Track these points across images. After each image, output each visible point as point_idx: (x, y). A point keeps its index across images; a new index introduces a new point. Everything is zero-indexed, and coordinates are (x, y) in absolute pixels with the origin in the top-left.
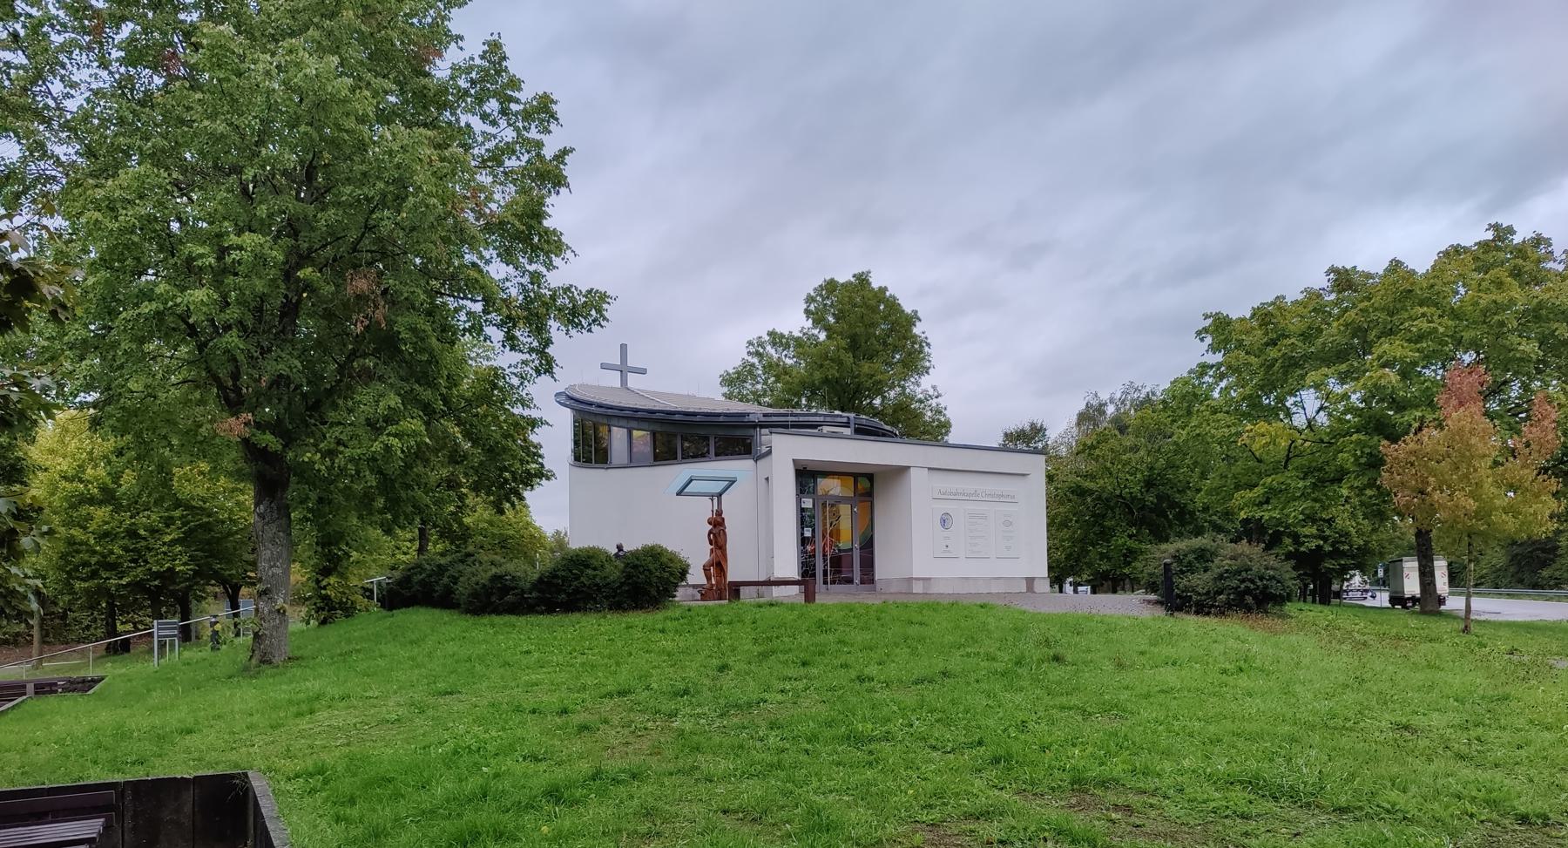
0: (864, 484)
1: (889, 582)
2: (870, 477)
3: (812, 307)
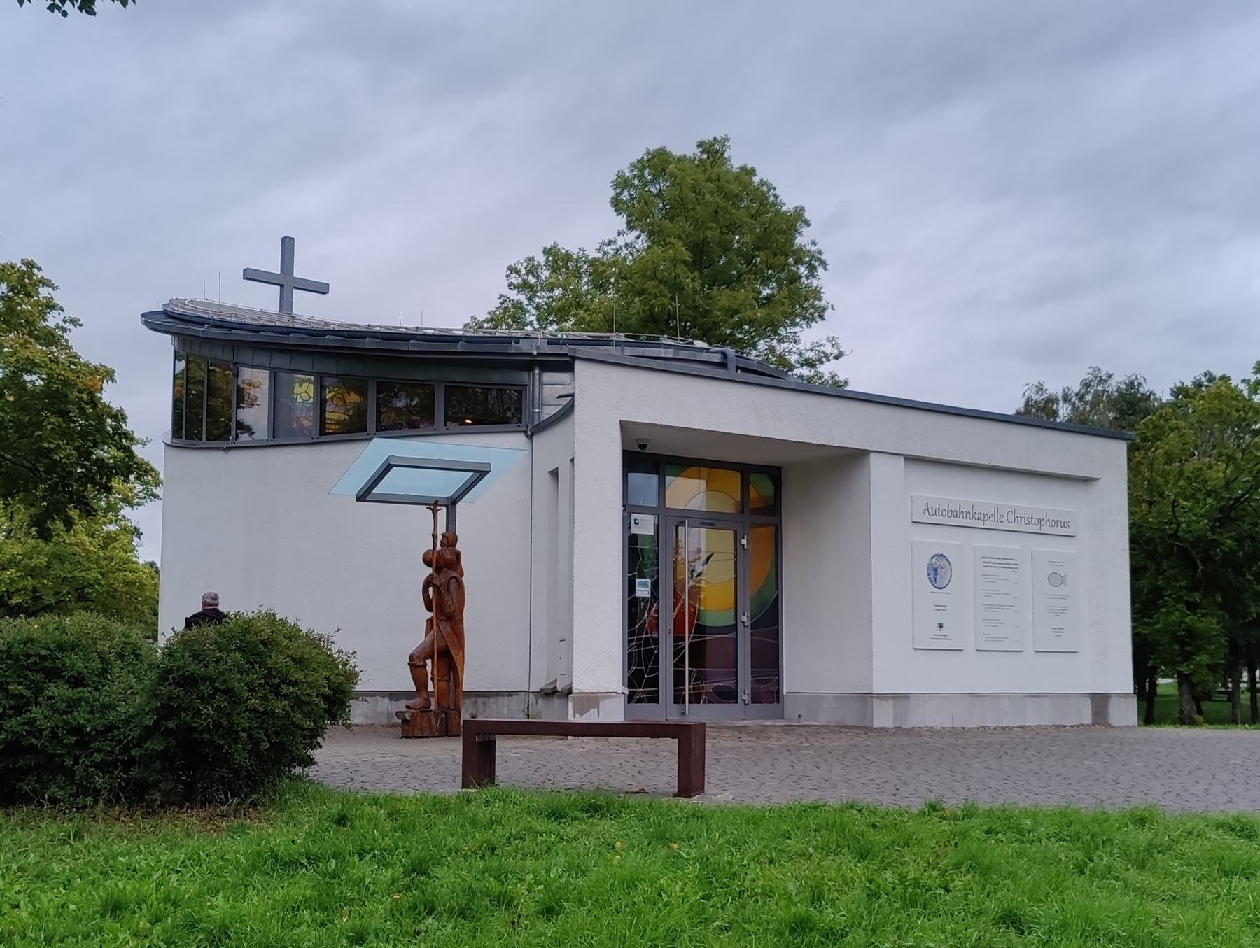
0: (761, 488)
1: (815, 700)
2: (775, 474)
3: (625, 196)
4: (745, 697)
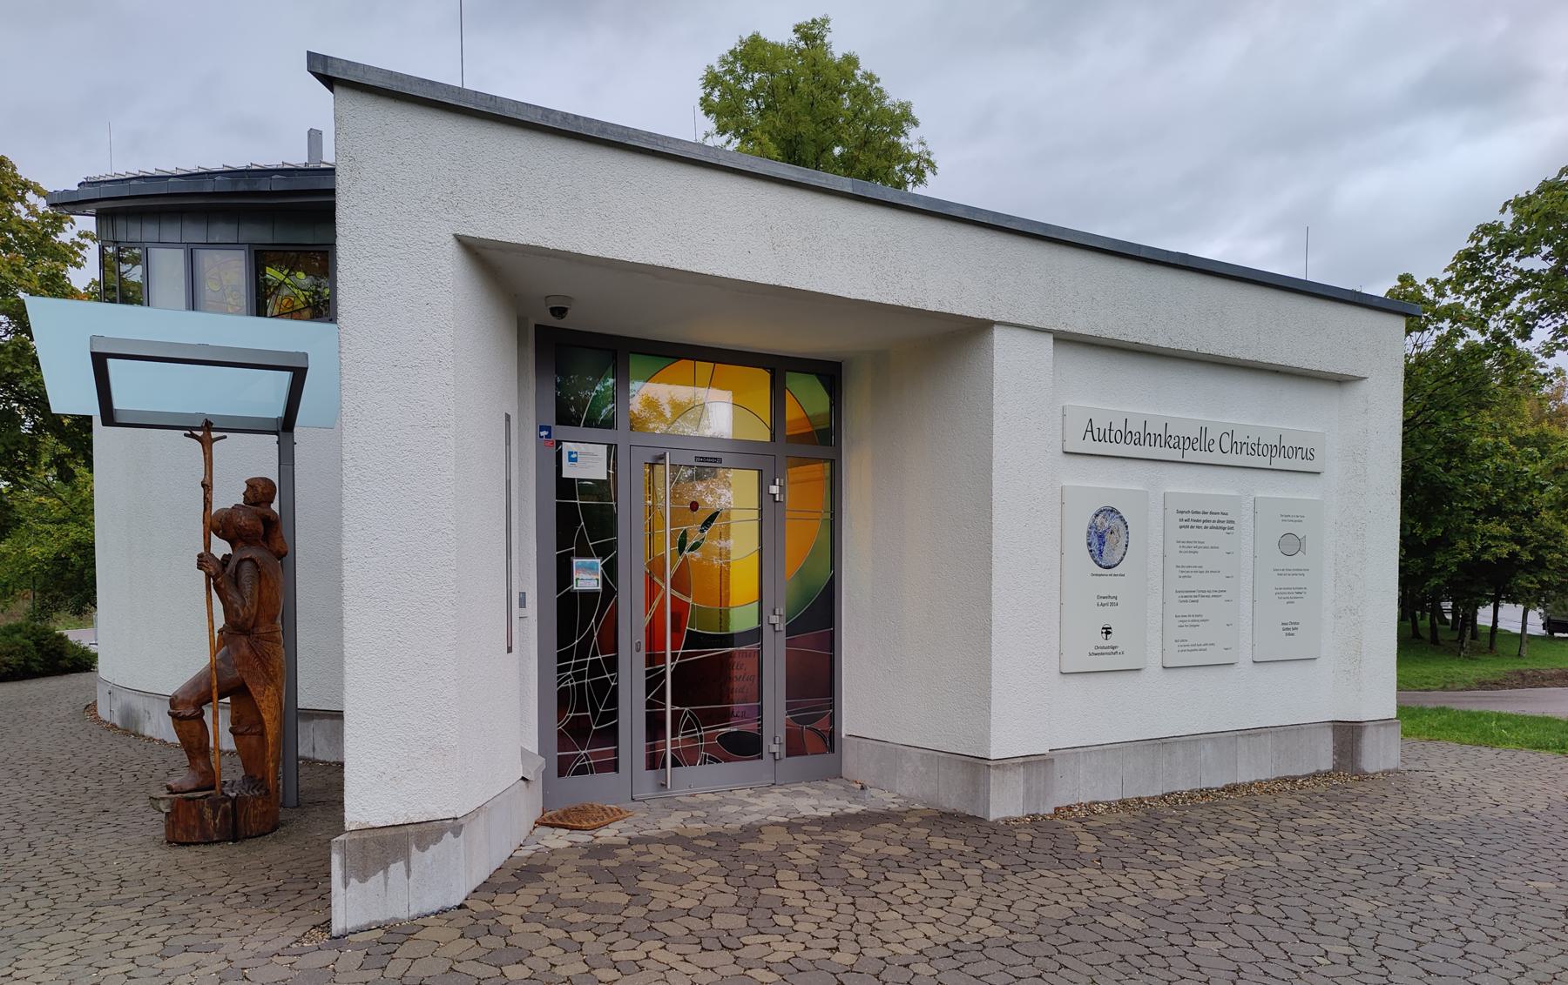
0: (806, 399)
1: (891, 754)
2: (830, 374)
4: (775, 748)
